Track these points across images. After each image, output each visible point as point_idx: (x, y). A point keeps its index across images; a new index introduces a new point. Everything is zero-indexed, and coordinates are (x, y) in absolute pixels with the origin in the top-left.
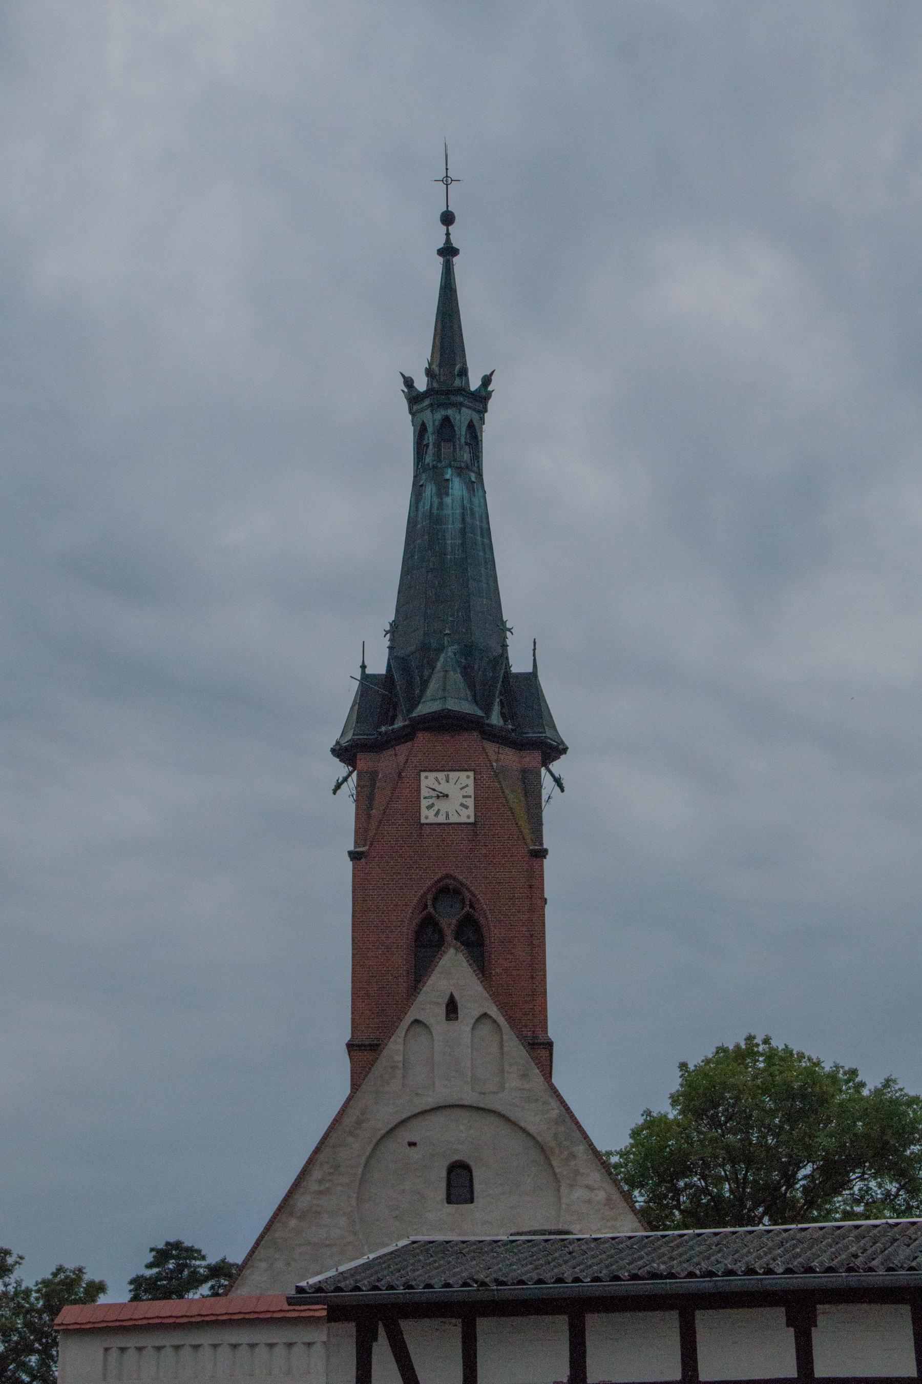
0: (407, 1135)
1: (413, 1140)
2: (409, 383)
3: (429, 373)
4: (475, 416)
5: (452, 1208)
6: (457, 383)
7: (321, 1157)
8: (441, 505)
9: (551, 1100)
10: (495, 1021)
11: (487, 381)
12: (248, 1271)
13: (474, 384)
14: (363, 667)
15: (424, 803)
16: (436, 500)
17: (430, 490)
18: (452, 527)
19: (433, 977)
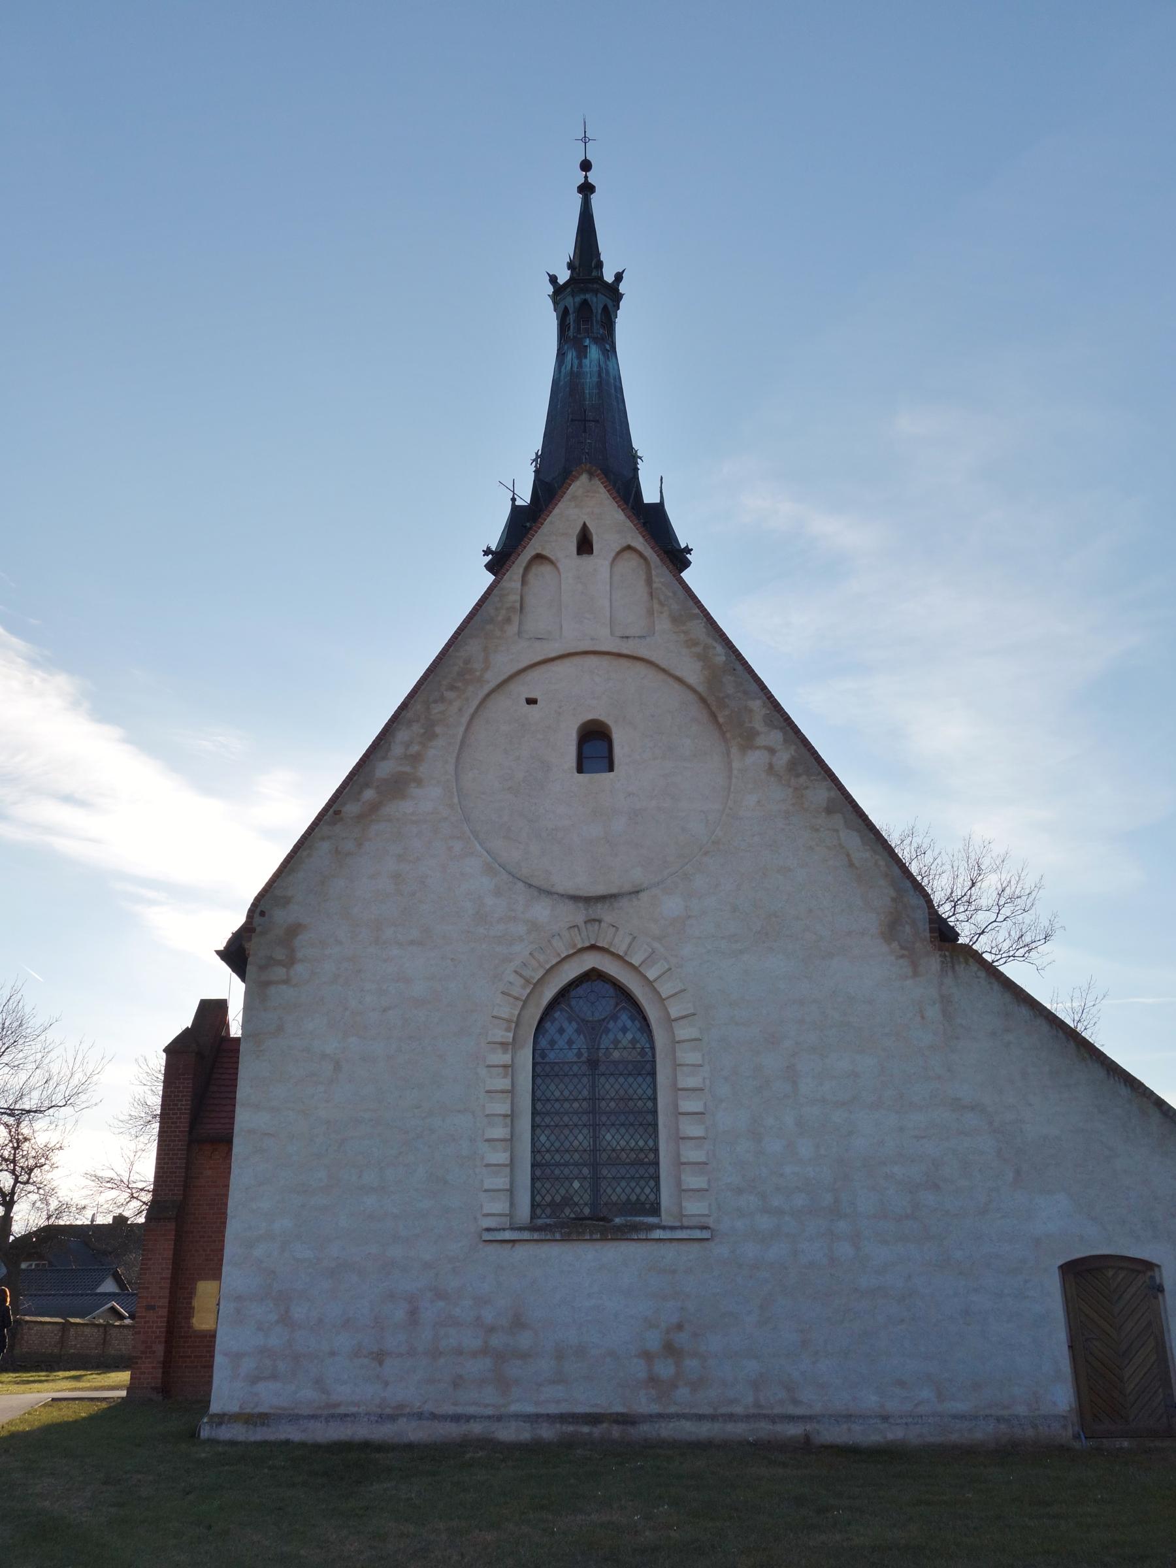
0: (522, 689)
1: (532, 696)
2: (553, 279)
3: (570, 266)
4: (610, 304)
5: (584, 778)
6: (594, 274)
7: (409, 714)
8: (580, 365)
9: (716, 645)
10: (641, 555)
11: (619, 277)
12: (305, 853)
13: (609, 277)
14: (514, 500)
16: (576, 362)
17: (571, 355)
18: (590, 380)
19: (560, 505)
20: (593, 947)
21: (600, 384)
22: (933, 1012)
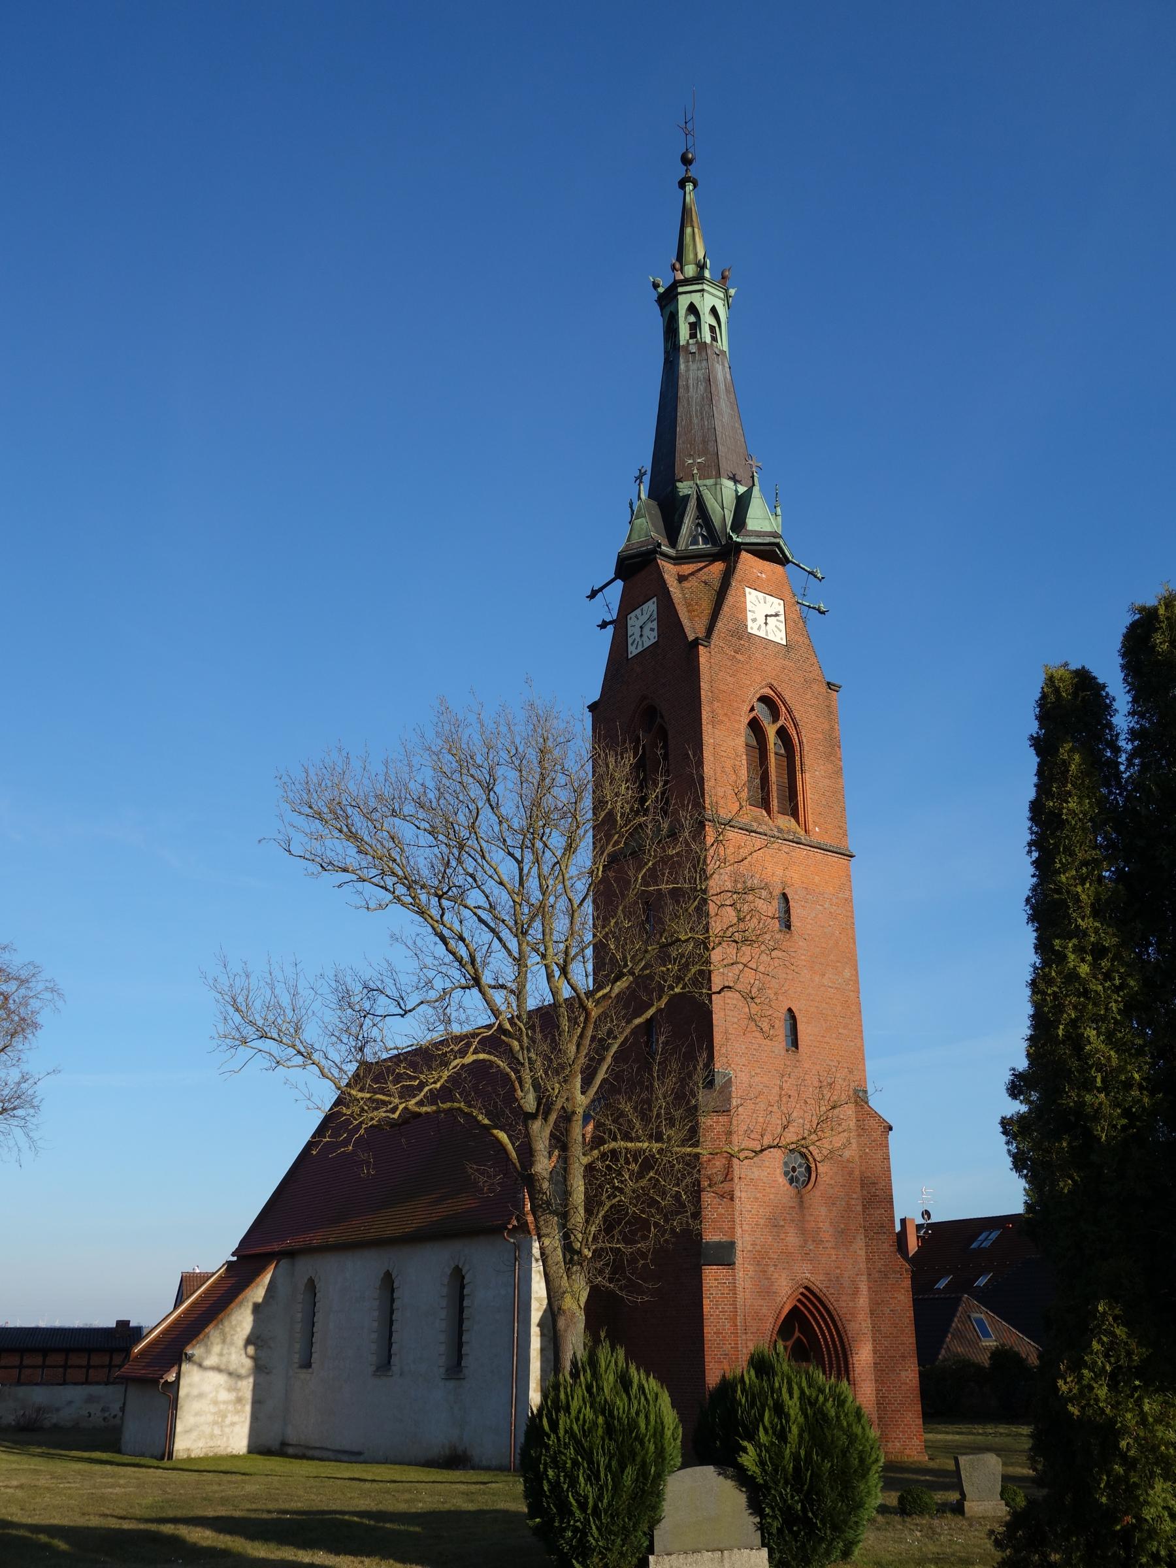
15: (750, 616)
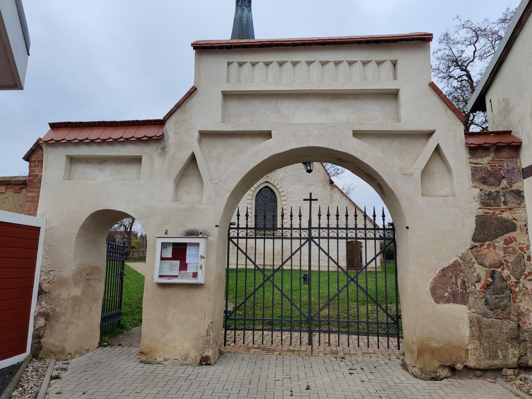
2: (508, 9)
17: (240, 11)
20: (267, 182)
21: (247, 20)
22: (328, 197)
